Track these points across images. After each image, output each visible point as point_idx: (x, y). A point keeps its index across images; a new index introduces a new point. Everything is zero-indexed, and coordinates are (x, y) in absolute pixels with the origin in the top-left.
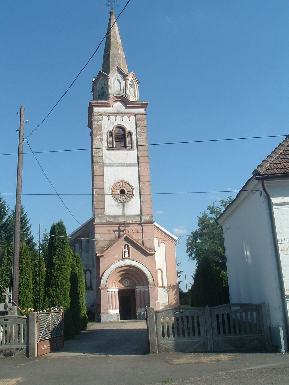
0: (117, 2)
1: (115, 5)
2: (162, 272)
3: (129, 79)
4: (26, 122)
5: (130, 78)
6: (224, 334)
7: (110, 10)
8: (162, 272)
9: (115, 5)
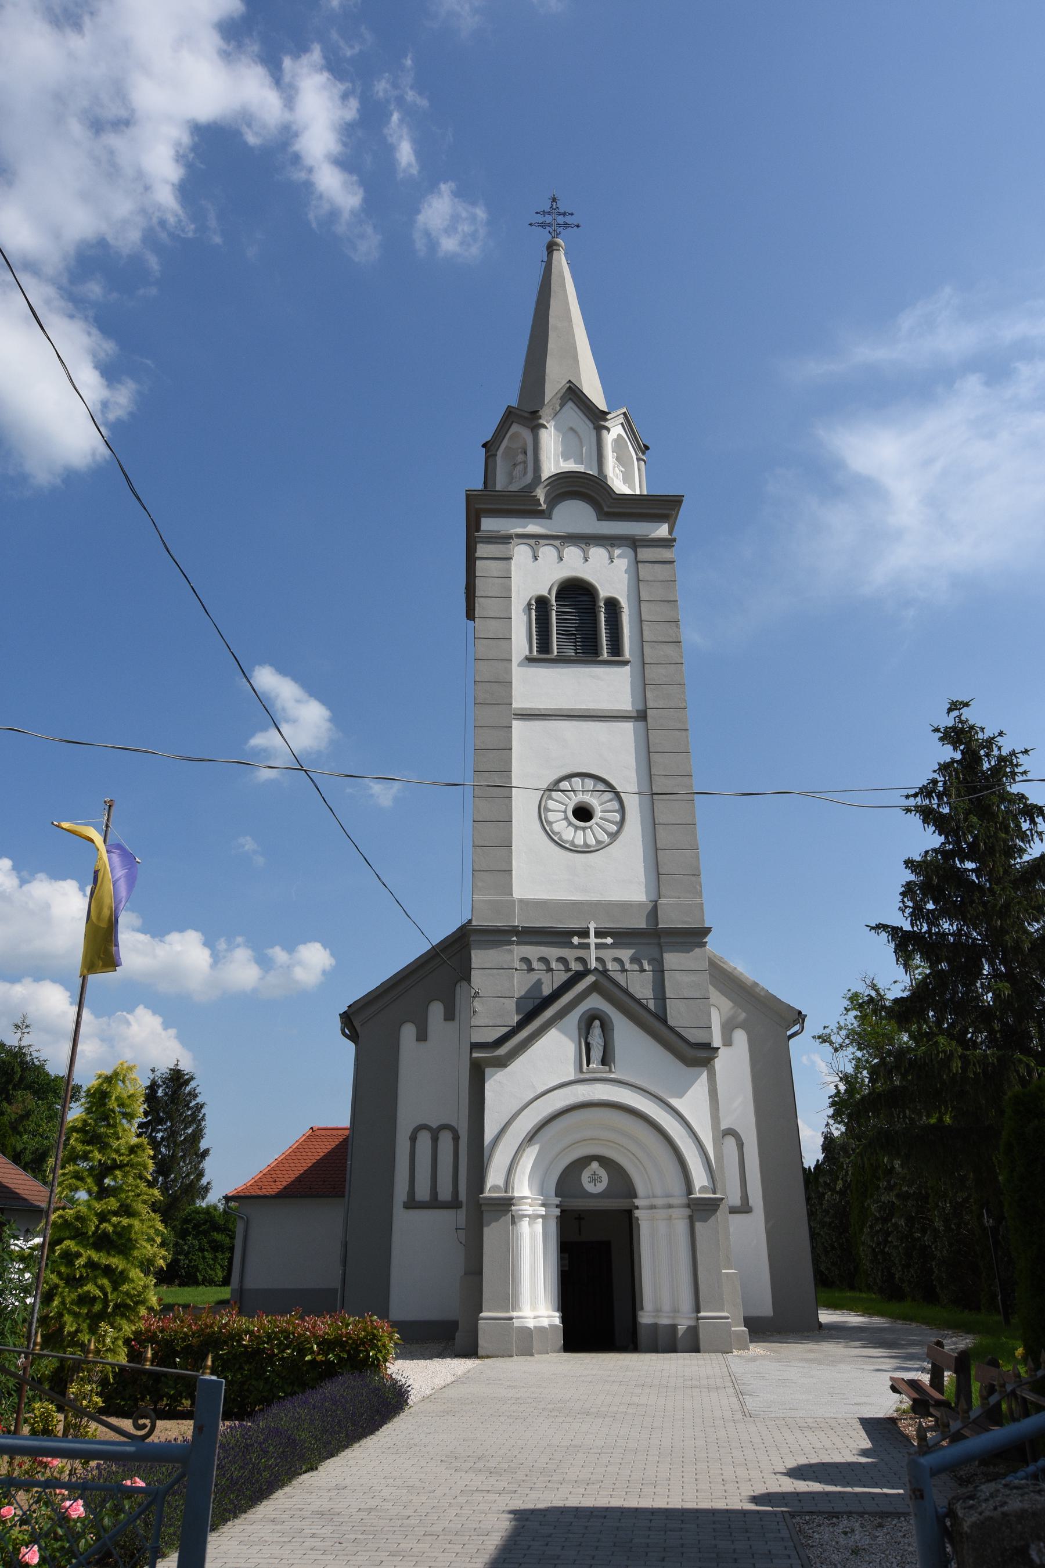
1: (566, 225)
2: (740, 1145)
5: (615, 430)
7: (549, 238)
8: (740, 1145)
9: (566, 225)
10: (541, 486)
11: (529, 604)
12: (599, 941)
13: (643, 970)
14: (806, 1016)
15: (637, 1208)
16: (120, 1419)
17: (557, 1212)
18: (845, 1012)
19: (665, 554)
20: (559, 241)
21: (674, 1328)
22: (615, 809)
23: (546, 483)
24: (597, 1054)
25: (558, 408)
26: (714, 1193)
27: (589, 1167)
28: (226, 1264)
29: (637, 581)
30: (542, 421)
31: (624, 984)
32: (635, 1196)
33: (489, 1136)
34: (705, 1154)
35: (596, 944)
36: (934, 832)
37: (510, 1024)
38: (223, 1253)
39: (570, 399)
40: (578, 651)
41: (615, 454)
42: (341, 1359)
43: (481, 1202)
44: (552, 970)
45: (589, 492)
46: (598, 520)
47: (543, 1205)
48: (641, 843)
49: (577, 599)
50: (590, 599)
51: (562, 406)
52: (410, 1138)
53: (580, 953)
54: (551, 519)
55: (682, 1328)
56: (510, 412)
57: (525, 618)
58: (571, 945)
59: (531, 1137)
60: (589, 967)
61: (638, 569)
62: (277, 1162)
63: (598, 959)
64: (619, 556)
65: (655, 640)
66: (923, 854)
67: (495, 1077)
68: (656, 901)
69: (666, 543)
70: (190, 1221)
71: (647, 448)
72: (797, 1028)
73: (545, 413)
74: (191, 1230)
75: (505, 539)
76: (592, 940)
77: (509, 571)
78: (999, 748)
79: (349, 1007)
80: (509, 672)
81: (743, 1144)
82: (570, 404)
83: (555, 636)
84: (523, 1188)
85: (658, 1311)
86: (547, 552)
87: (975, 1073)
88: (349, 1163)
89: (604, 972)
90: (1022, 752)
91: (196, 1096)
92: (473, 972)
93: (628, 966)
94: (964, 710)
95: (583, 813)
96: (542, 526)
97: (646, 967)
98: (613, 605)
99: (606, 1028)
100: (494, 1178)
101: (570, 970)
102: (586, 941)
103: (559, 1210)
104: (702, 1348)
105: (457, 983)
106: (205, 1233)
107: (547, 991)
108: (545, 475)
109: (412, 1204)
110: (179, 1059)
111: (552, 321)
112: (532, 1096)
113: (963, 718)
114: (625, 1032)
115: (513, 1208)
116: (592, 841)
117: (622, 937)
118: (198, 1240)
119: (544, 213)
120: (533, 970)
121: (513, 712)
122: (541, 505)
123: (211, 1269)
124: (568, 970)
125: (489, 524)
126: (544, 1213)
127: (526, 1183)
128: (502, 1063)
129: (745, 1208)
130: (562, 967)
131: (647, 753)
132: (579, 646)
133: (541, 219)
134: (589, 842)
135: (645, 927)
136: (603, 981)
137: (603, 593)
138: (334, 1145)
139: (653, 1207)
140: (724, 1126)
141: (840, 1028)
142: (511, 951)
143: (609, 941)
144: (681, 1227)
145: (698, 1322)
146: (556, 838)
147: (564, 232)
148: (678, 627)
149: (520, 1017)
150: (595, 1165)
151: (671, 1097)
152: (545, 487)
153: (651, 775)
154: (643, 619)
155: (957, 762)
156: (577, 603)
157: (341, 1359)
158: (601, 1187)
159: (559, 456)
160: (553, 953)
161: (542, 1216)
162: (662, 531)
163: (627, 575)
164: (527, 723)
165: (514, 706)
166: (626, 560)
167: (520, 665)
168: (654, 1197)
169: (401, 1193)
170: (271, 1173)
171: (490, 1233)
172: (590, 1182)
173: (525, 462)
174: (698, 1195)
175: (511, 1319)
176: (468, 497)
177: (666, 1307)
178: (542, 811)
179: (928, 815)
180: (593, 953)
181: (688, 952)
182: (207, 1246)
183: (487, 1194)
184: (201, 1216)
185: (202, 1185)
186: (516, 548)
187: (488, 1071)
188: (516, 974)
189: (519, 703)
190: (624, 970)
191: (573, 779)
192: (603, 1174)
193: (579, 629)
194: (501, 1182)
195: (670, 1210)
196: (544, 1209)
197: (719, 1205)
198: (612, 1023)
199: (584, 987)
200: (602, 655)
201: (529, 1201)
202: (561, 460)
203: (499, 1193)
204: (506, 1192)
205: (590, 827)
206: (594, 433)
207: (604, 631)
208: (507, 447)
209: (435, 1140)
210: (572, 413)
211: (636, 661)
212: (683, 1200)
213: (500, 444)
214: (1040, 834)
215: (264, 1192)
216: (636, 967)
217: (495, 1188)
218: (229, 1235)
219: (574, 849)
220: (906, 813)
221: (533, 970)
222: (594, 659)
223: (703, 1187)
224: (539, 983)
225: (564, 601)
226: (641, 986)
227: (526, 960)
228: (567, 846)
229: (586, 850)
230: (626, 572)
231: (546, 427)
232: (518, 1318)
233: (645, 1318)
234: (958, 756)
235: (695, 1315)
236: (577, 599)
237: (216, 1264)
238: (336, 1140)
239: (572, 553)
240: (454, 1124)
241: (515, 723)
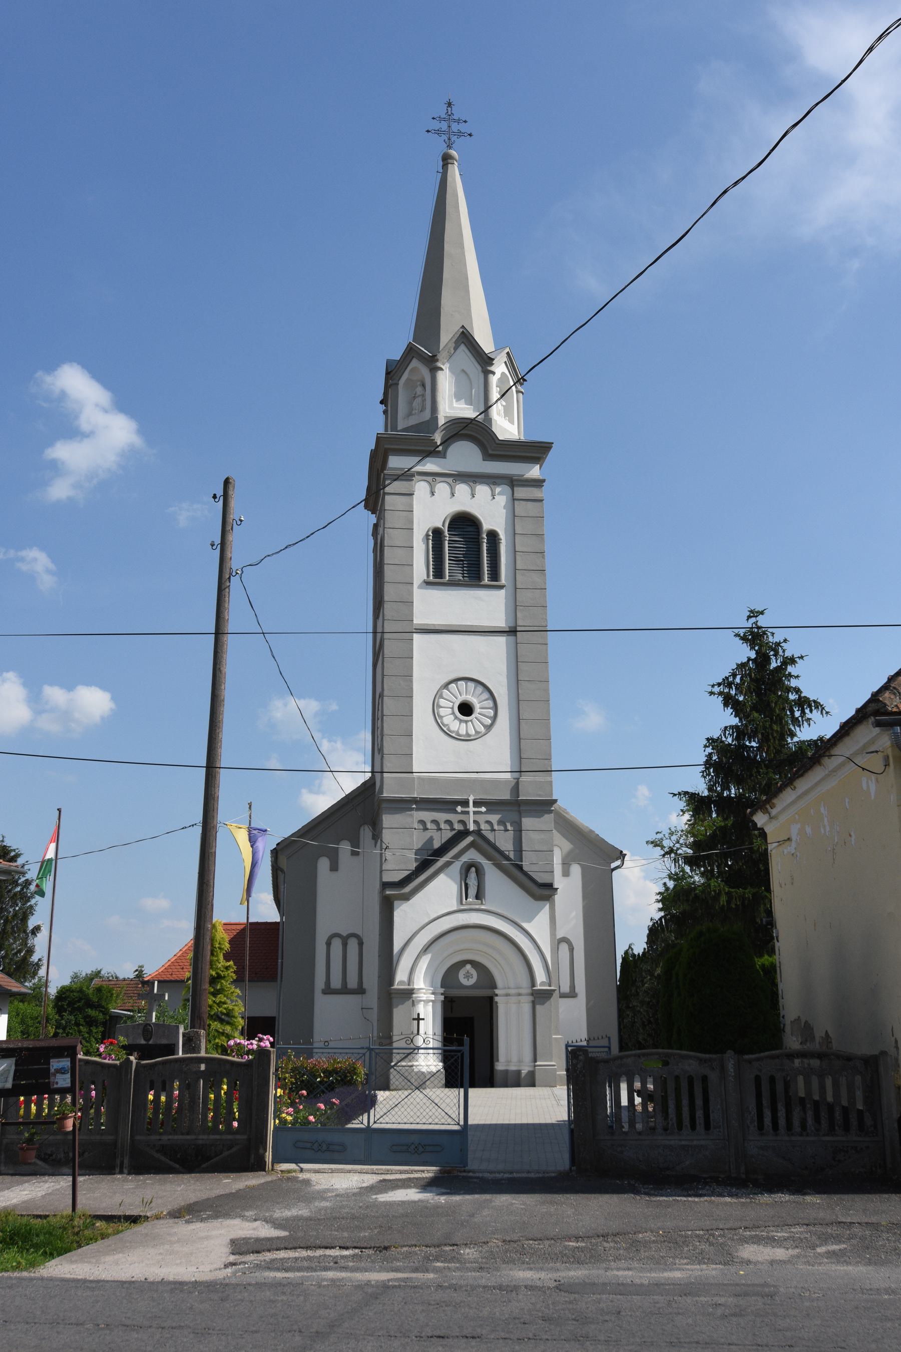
0: (465, 122)
1: (460, 134)
2: (571, 950)
3: (496, 371)
4: (239, 523)
5: (500, 368)
6: (788, 1130)
7: (443, 148)
8: (571, 950)
9: (460, 134)
10: (439, 431)
11: (427, 535)
12: (476, 809)
13: (506, 830)
14: (626, 855)
15: (497, 995)
17: (442, 998)
18: (681, 813)
19: (534, 493)
20: (453, 153)
21: (519, 1072)
22: (489, 715)
23: (443, 428)
24: (472, 891)
26: (550, 986)
27: (464, 968)
28: (100, 1037)
29: (513, 516)
30: (439, 364)
31: (493, 840)
32: (496, 988)
33: (397, 947)
34: (544, 957)
35: (473, 812)
36: (732, 714)
37: (411, 869)
38: (97, 1027)
39: (463, 342)
40: (465, 575)
41: (498, 389)
42: (337, 1080)
43: (392, 991)
44: (441, 829)
45: (478, 436)
46: (484, 460)
47: (433, 993)
49: (465, 530)
50: (475, 530)
51: (455, 349)
53: (462, 817)
54: (445, 458)
55: (524, 1072)
57: (423, 547)
59: (426, 949)
60: (468, 827)
61: (515, 538)
62: (182, 952)
63: (475, 822)
64: (499, 494)
65: (526, 568)
66: (723, 728)
67: (401, 907)
68: (518, 779)
69: (538, 483)
70: (65, 998)
72: (618, 863)
73: (442, 356)
74: (66, 1007)
75: (407, 476)
76: (471, 809)
77: (411, 506)
78: (784, 651)
79: (278, 845)
80: (411, 593)
81: (573, 949)
82: (463, 347)
83: (447, 562)
84: (420, 983)
85: (508, 1062)
86: (442, 488)
87: (736, 905)
88: (280, 961)
89: (478, 832)
90: (799, 657)
91: (24, 874)
92: (384, 831)
93: (496, 827)
94: (760, 617)
95: (466, 709)
96: (438, 465)
97: (509, 827)
98: (493, 536)
99: (480, 873)
100: (401, 976)
101: (454, 829)
102: (466, 809)
103: (443, 997)
104: (537, 1084)
105: (361, 826)
106: (80, 1009)
107: (437, 845)
108: (441, 421)
109: (328, 990)
110: (4, 835)
111: (447, 247)
112: (427, 920)
113: (759, 624)
114: (494, 878)
115: (414, 995)
116: (472, 732)
117: (492, 805)
118: (75, 1016)
119: (441, 119)
120: (427, 829)
121: (414, 627)
122: (503, 374)
123: (87, 1042)
124: (452, 829)
125: (396, 462)
126: (433, 999)
127: (422, 979)
128: (406, 898)
129: (572, 994)
130: (448, 827)
131: (516, 662)
132: (466, 570)
133: (436, 125)
134: (470, 732)
135: (509, 798)
136: (480, 841)
137: (486, 526)
139: (507, 995)
140: (559, 935)
141: (672, 834)
142: (412, 816)
143: (483, 809)
144: (526, 1008)
145: (535, 1069)
146: (445, 729)
147: (458, 142)
148: (543, 557)
149: (418, 864)
150: (468, 967)
151: (523, 922)
152: (443, 431)
153: (518, 680)
154: (517, 550)
155: (752, 660)
156: (465, 533)
157: (337, 1080)
158: (472, 981)
159: (452, 397)
160: (441, 817)
161: (432, 1001)
162: (534, 472)
163: (505, 511)
165: (415, 622)
166: (505, 497)
167: (420, 587)
168: (509, 988)
169: (320, 983)
171: (399, 1013)
172: (464, 978)
173: (423, 395)
174: (539, 988)
175: (412, 1066)
176: (378, 438)
177: (515, 1059)
178: (435, 706)
179: (728, 700)
180: (472, 817)
181: (539, 817)
182: (82, 1021)
183: (396, 986)
184: (75, 994)
185: (33, 962)
186: (417, 484)
187: (396, 903)
188: (415, 832)
189: (419, 619)
190: (493, 830)
191: (459, 683)
192: (474, 973)
193: (465, 556)
194: (405, 979)
195: (520, 997)
196: (433, 996)
197: (552, 994)
198: (484, 869)
199: (465, 845)
200: (484, 580)
201: (424, 991)
202: (454, 400)
203: (404, 985)
204: (409, 985)
205: (471, 721)
206: (482, 376)
207: (485, 558)
208: (407, 379)
209: (345, 945)
210: (463, 354)
211: (510, 586)
212: (529, 991)
213: (402, 375)
214: (809, 720)
216: (502, 828)
217: (401, 983)
218: (101, 1011)
219: (458, 738)
220: (710, 695)
221: (427, 829)
222: (477, 583)
223: (543, 982)
224: (431, 839)
225: (454, 531)
226: (505, 842)
227: (422, 822)
228: (453, 735)
229: (467, 739)
231: (441, 369)
232: (416, 1066)
233: (500, 1066)
234: (753, 655)
235: (533, 1064)
236: (465, 530)
237: (92, 1037)
238: (231, 934)
239: (462, 489)
240: (360, 933)
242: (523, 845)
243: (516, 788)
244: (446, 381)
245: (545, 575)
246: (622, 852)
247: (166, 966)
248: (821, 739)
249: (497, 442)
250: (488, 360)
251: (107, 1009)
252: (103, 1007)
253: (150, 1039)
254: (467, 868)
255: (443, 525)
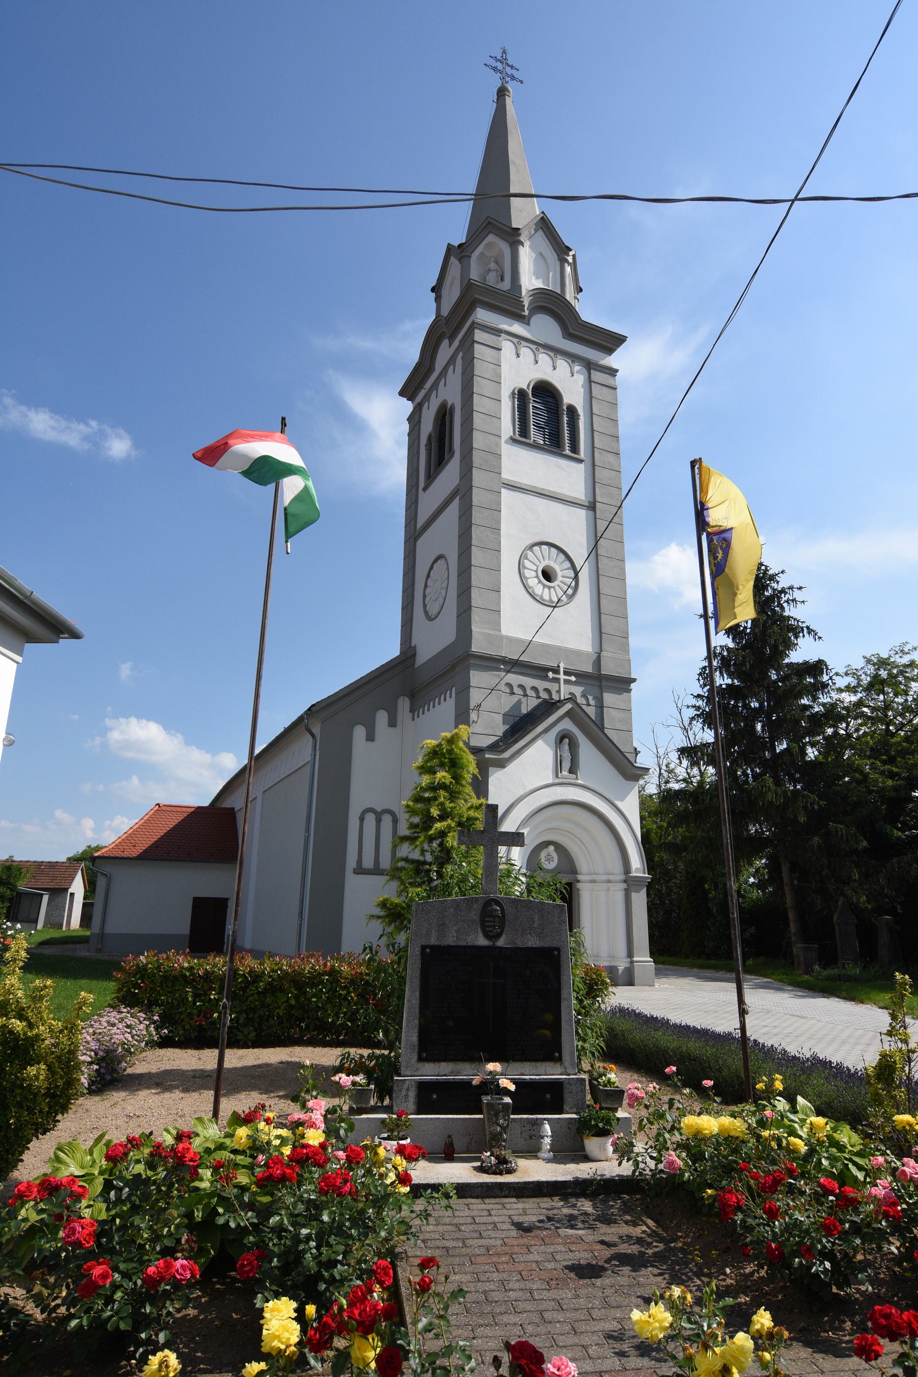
11: (513, 393)
15: (578, 881)
16: (628, 1075)
24: (567, 765)
25: (533, 232)
29: (590, 397)
37: (471, 741)
39: (541, 228)
48: (589, 606)
52: (360, 818)
56: (489, 223)
58: (546, 678)
65: (602, 448)
71: (581, 290)
76: (562, 677)
80: (499, 446)
82: (540, 232)
86: (526, 352)
95: (548, 575)
98: (572, 410)
101: (540, 698)
102: (557, 676)
104: (636, 981)
109: (360, 870)
117: (581, 677)
119: (497, 60)
122: (524, 311)
124: (538, 697)
128: (502, 764)
133: (494, 64)
137: (567, 400)
138: (180, 819)
143: (573, 678)
148: (618, 441)
149: (507, 727)
150: (552, 848)
160: (529, 682)
164: (511, 492)
165: (503, 476)
167: (506, 442)
170: (130, 838)
177: (604, 953)
178: (521, 567)
187: (491, 769)
206: (558, 263)
208: (482, 254)
209: (379, 821)
211: (588, 460)
212: (623, 877)
215: (126, 854)
230: (583, 386)
241: (503, 491)
242: (605, 722)
243: (598, 662)
244: (526, 256)
245: (619, 458)
246: (636, 749)
247: (117, 843)
248: (806, 663)
249: (580, 322)
250: (565, 249)
251: (15, 887)
252: (11, 884)
253: (499, 935)
254: (563, 737)
255: (528, 388)
